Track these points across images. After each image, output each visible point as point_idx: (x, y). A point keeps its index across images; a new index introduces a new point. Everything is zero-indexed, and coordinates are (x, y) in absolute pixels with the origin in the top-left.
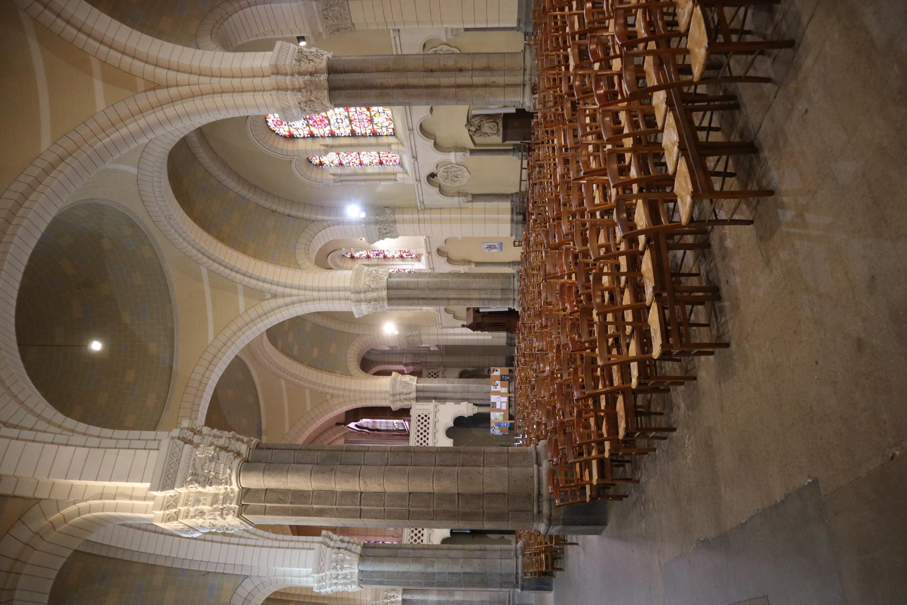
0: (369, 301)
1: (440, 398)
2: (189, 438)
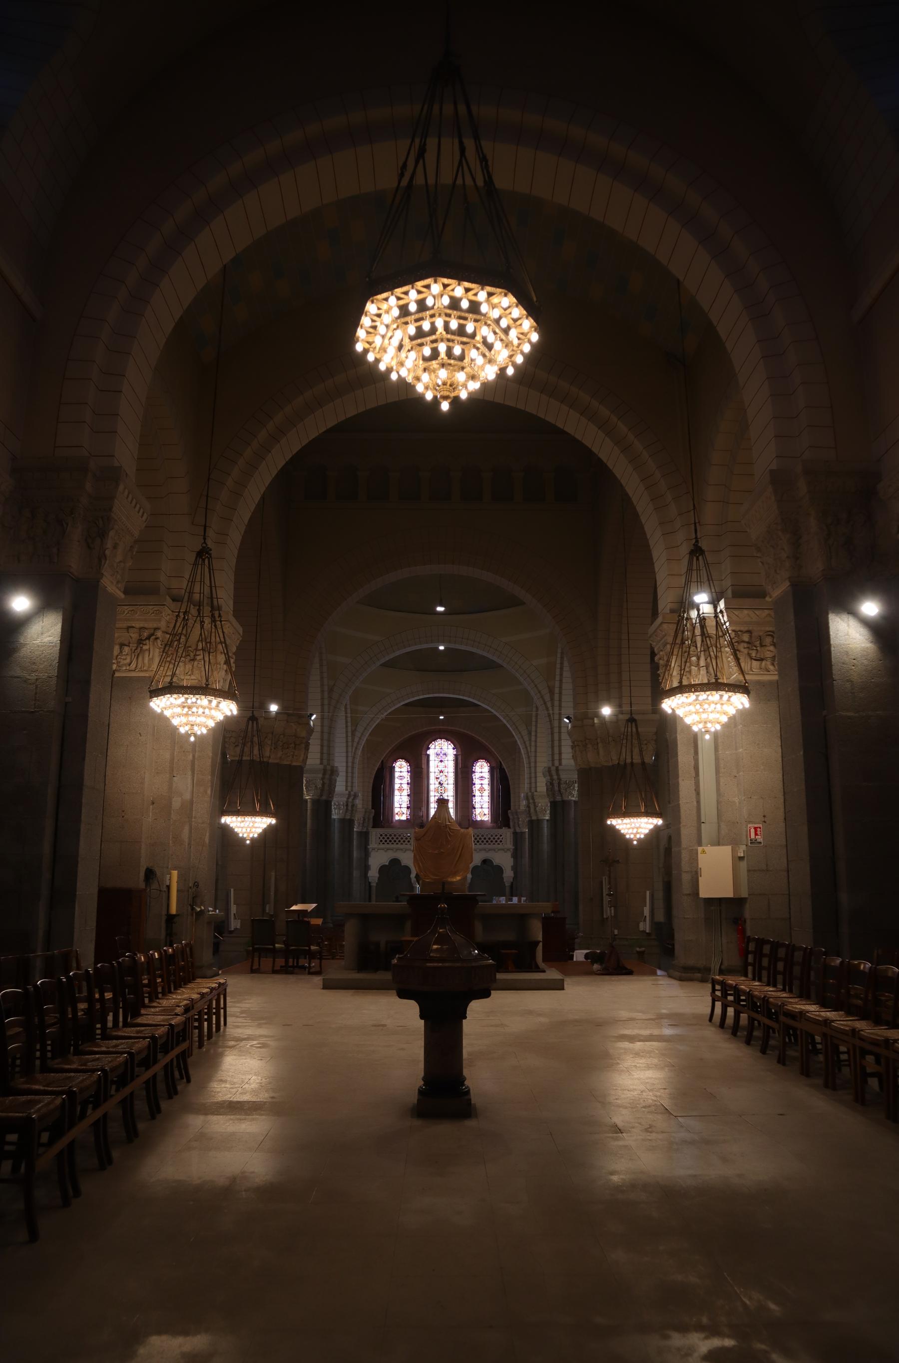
0: (528, 807)
1: (516, 855)
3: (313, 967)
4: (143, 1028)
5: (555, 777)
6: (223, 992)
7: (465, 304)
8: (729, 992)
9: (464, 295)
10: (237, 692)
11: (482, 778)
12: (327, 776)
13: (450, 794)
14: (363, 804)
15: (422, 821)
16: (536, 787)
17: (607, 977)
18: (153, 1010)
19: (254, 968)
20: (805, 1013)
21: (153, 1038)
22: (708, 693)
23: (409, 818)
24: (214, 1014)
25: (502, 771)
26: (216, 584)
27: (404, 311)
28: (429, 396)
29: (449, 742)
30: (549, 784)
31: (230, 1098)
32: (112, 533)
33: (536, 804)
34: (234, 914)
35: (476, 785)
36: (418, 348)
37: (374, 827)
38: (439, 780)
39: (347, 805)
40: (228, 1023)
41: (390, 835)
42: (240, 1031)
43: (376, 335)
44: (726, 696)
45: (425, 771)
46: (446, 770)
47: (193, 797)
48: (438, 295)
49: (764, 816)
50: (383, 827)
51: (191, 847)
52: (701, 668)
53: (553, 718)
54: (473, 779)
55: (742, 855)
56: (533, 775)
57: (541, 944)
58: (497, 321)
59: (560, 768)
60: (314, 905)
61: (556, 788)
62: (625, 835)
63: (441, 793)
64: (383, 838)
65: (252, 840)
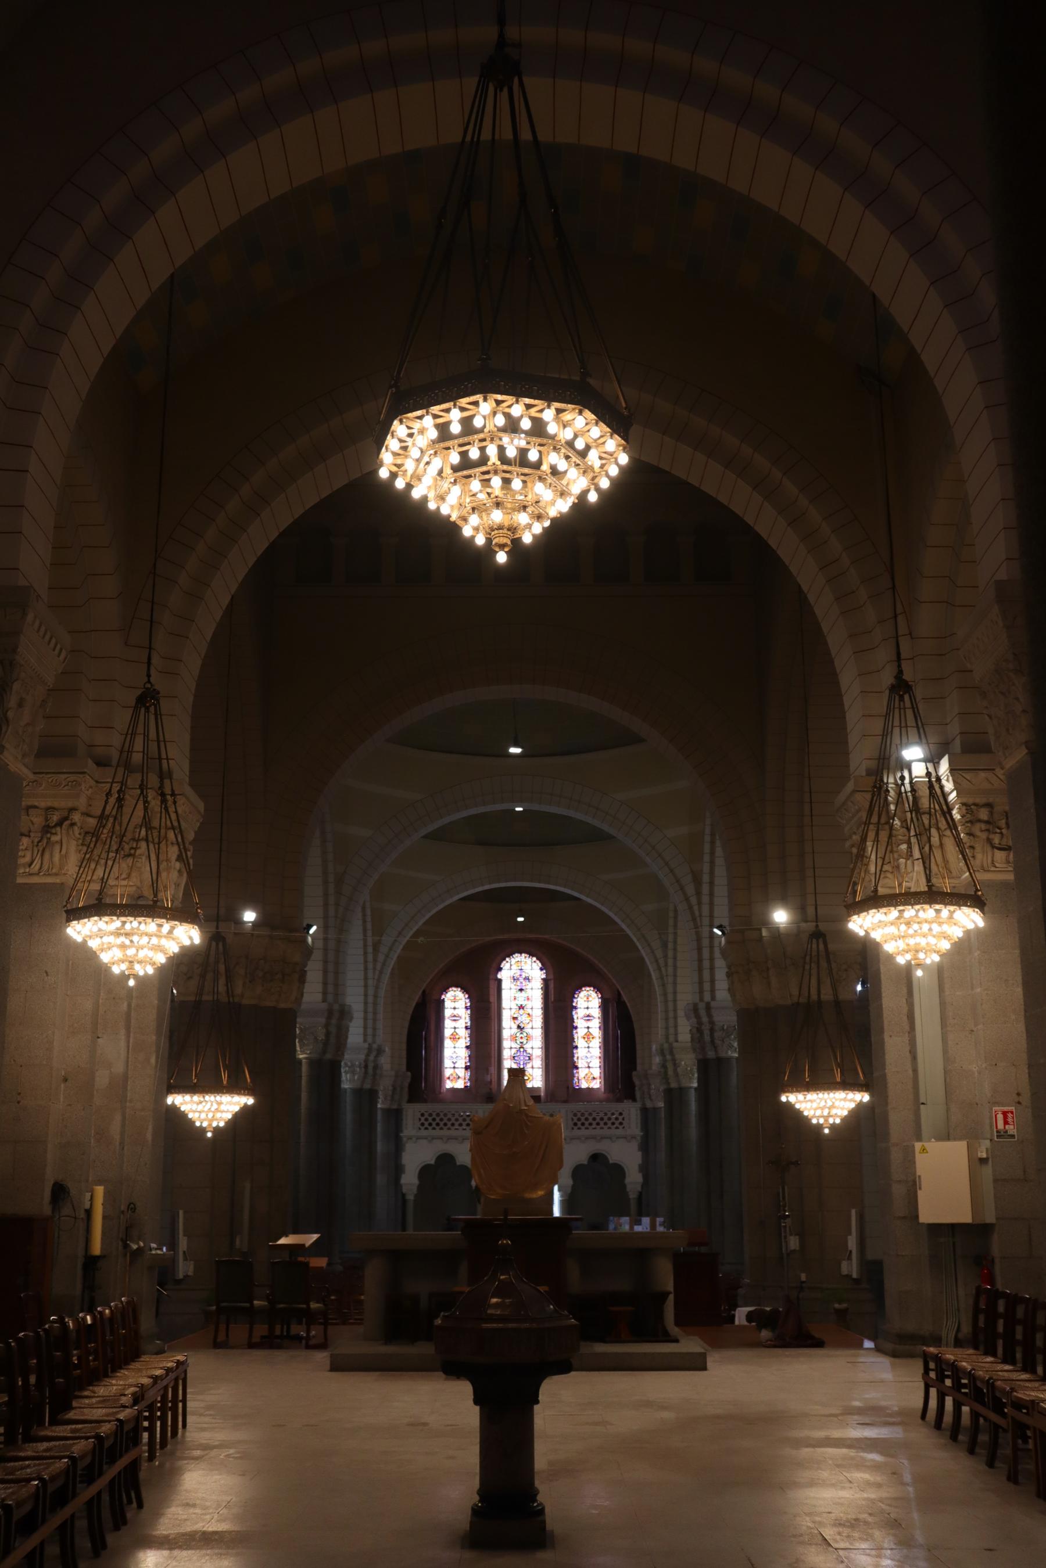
0: (664, 1066)
1: (646, 1146)
3: (314, 1337)
4: (80, 1426)
5: (705, 1019)
6: (183, 1376)
7: (526, 424)
8: (946, 1373)
9: (525, 413)
10: (199, 911)
11: (588, 1017)
12: (334, 1021)
13: (536, 1045)
15: (491, 1089)
16: (676, 1034)
17: (779, 1351)
18: (87, 1402)
19: (219, 1340)
20: (1038, 1403)
21: (98, 1437)
22: (917, 907)
23: (468, 1084)
24: (170, 1409)
25: (621, 1005)
26: (166, 737)
27: (443, 429)
28: (480, 540)
29: (534, 959)
30: (695, 1030)
31: (204, 1527)
32: (16, 686)
34: (184, 1252)
35: (578, 1030)
36: (464, 480)
37: (410, 1101)
38: (517, 1022)
39: (366, 1067)
40: (188, 1425)
41: (438, 1115)
42: (206, 1435)
43: (406, 457)
44: (945, 911)
45: (494, 1006)
46: (529, 1004)
47: (128, 1069)
48: (489, 415)
49: (1018, 1094)
50: (425, 1101)
51: (123, 1149)
52: (916, 862)
54: (573, 1019)
55: (984, 1155)
56: (671, 1014)
57: (671, 1297)
58: (570, 444)
59: (713, 1004)
60: (315, 1236)
61: (707, 1038)
62: (810, 1120)
63: (521, 1043)
64: (426, 1120)
65: (217, 1130)
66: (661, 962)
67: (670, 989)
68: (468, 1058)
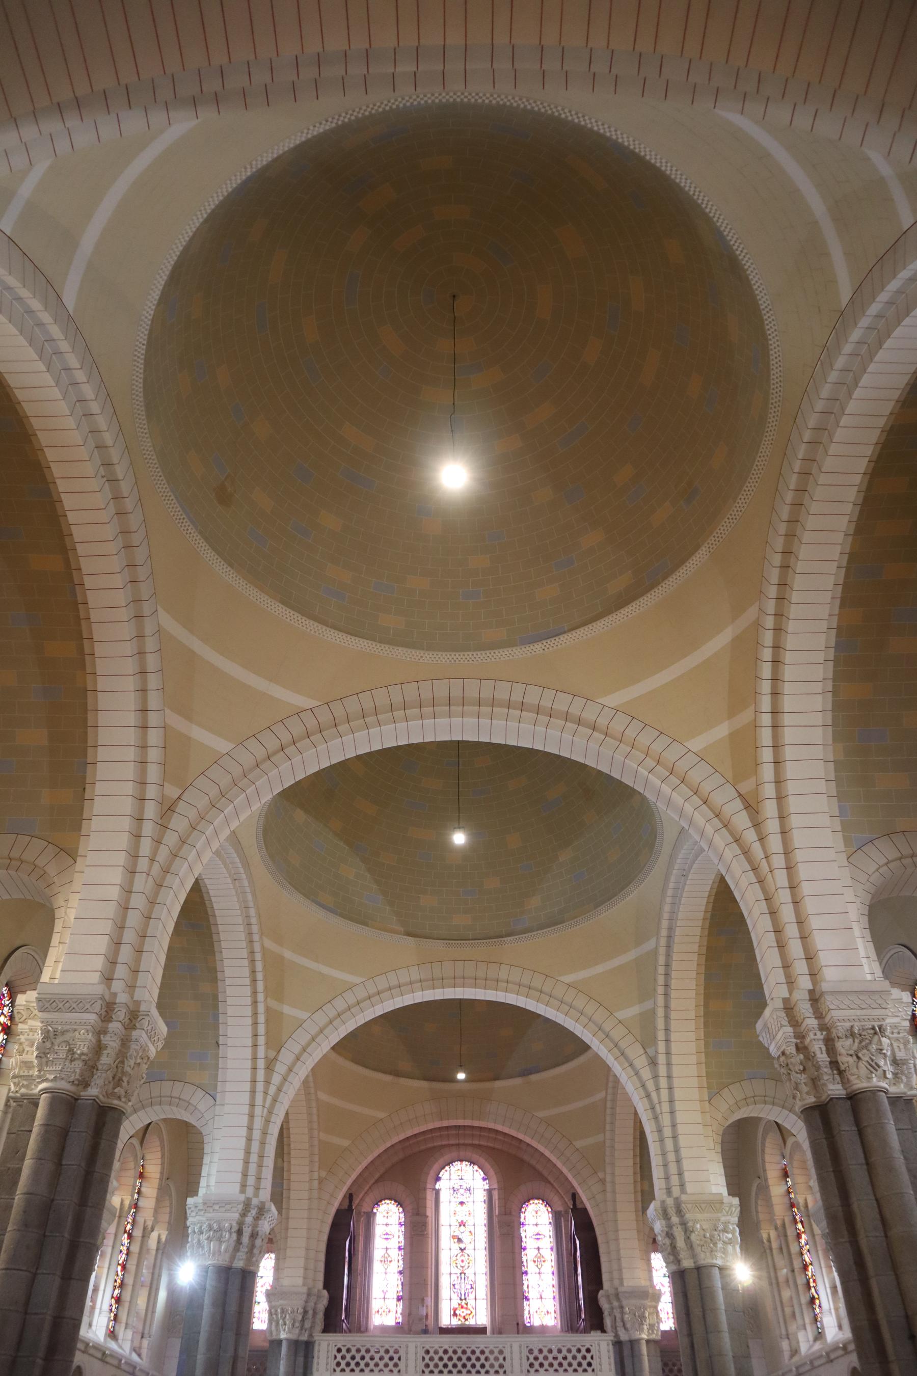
2: (113, 1017)
14: (305, 1278)
15: (426, 1326)
23: (400, 1320)
29: (476, 1167)
33: (690, 1224)
37: (326, 1329)
39: (240, 1232)
46: (470, 1221)
53: (661, 1110)
54: (521, 1238)
63: (462, 1267)
66: (650, 1085)
67: (666, 1120)
68: (400, 1287)
